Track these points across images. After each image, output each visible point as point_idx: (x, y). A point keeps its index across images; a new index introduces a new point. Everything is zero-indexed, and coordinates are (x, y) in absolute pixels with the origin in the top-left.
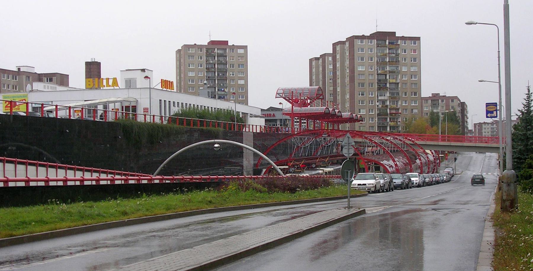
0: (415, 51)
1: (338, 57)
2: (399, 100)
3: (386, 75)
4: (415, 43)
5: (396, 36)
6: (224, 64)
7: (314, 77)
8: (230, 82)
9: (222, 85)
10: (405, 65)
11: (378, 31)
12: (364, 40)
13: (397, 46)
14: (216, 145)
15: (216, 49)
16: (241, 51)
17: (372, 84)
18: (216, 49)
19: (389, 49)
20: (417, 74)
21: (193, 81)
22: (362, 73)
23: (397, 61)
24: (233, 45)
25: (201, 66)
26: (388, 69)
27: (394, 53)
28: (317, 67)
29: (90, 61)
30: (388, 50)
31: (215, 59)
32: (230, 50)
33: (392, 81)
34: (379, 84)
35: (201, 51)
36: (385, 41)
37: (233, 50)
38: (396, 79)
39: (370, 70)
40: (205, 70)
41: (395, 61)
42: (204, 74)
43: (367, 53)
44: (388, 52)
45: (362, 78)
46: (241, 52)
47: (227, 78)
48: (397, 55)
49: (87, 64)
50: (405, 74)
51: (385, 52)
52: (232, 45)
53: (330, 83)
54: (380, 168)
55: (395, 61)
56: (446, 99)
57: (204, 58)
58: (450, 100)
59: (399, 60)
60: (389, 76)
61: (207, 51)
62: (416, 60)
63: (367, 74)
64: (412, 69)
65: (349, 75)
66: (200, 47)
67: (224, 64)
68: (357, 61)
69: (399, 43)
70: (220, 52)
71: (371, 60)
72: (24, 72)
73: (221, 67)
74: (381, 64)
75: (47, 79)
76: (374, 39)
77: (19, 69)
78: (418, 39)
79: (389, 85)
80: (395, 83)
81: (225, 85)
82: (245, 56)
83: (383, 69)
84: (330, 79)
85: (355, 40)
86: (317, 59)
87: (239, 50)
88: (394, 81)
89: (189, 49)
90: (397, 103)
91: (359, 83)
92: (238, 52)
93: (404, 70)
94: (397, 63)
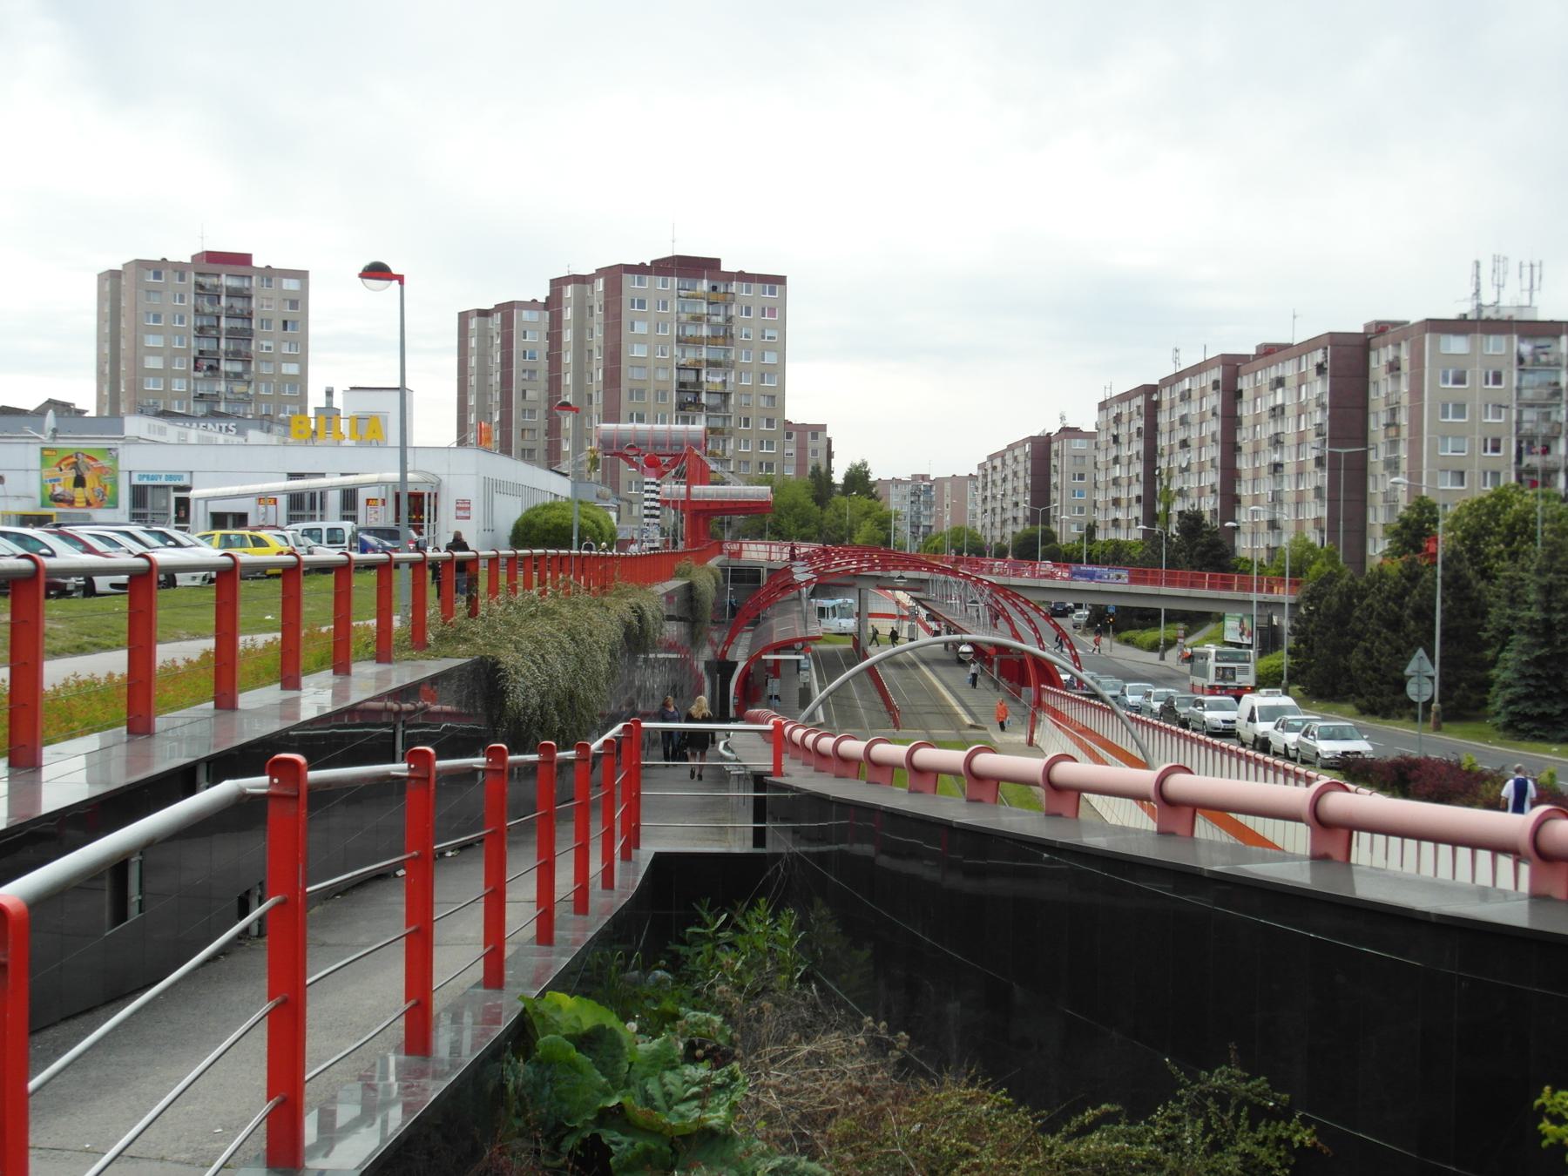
0: (772, 312)
1: (568, 314)
2: (730, 438)
4: (772, 292)
5: (722, 269)
11: (676, 254)
12: (647, 277)
17: (664, 394)
19: (709, 303)
22: (640, 364)
24: (269, 267)
25: (181, 321)
28: (484, 335)
30: (705, 305)
31: (219, 303)
32: (263, 280)
35: (182, 278)
37: (269, 280)
39: (659, 356)
40: (193, 332)
42: (189, 344)
45: (636, 374)
46: (291, 281)
48: (729, 319)
52: (263, 266)
53: (524, 380)
54: (489, 589)
55: (724, 336)
56: (797, 431)
58: (809, 434)
59: (734, 332)
66: (180, 269)
73: (238, 324)
78: (781, 280)
79: (707, 398)
82: (298, 303)
84: (524, 371)
86: (483, 314)
90: (724, 446)
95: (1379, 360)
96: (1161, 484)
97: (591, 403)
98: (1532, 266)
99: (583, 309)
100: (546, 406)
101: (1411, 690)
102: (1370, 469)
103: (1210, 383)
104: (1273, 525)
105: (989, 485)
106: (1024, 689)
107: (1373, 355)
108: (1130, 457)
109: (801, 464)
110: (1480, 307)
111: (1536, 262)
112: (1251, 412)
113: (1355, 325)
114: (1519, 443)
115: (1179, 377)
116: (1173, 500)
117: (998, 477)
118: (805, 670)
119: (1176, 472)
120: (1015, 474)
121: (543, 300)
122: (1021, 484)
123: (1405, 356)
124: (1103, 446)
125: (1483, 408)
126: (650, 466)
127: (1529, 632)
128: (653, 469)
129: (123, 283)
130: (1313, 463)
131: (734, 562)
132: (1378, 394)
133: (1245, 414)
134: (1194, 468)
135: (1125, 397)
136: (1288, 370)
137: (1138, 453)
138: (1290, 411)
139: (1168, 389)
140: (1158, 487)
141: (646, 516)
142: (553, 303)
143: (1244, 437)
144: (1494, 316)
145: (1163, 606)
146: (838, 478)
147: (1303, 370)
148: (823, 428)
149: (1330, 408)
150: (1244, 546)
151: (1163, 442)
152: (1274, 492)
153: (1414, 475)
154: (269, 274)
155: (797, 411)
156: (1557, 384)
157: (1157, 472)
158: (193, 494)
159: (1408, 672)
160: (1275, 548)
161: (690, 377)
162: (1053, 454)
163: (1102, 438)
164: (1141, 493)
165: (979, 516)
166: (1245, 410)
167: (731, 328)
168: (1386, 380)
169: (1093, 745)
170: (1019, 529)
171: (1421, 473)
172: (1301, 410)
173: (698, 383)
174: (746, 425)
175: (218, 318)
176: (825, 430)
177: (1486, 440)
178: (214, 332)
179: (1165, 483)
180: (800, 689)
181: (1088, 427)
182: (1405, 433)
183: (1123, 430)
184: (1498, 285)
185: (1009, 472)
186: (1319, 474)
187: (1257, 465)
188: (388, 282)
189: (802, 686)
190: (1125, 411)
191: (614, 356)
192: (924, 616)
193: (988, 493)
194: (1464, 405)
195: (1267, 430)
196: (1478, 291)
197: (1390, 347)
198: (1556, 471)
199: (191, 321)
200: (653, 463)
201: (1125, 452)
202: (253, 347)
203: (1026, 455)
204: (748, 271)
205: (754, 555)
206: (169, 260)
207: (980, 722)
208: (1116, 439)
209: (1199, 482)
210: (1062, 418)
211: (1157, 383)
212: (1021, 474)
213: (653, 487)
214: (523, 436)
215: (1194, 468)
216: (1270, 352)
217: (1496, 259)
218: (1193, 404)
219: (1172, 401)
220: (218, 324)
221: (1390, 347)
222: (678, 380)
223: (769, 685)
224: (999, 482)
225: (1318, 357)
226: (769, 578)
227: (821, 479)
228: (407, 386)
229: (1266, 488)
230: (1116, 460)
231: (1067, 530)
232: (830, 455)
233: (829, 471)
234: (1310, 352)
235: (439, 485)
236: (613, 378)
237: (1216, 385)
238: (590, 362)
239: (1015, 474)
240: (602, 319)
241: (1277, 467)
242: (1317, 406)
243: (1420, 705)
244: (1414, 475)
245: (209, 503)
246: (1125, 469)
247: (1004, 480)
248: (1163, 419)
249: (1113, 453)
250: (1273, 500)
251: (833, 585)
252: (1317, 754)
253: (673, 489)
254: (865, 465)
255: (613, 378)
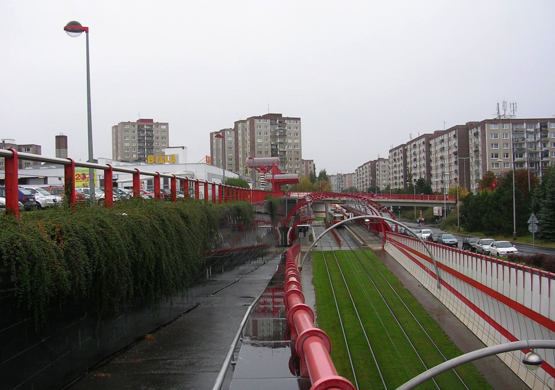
0: (297, 128)
1: (240, 132)
3: (277, 146)
4: (297, 123)
6: (151, 137)
7: (214, 146)
8: (156, 150)
9: (149, 152)
10: (290, 138)
13: (285, 124)
14: (367, 220)
15: (145, 126)
16: (164, 127)
17: (267, 152)
18: (145, 126)
19: (279, 126)
20: (299, 145)
21: (128, 150)
22: (260, 144)
23: (285, 136)
25: (134, 139)
26: (278, 141)
27: (282, 130)
29: (58, 135)
30: (278, 127)
33: (281, 150)
34: (272, 152)
35: (134, 127)
36: (276, 121)
37: (158, 126)
38: (284, 149)
41: (283, 135)
42: (136, 145)
43: (263, 129)
44: (278, 128)
45: (260, 147)
46: (164, 128)
47: (153, 147)
49: (57, 137)
50: (290, 145)
51: (276, 129)
52: (156, 122)
55: (283, 136)
57: (136, 132)
58: (309, 163)
60: (279, 146)
61: (138, 127)
62: (298, 135)
63: (264, 145)
64: (296, 141)
65: (249, 145)
66: (133, 124)
67: (151, 137)
68: (257, 135)
69: (286, 122)
70: (148, 127)
71: (267, 135)
72: (9, 144)
73: (150, 139)
74: (274, 137)
75: (25, 149)
76: (268, 119)
77: (4, 142)
78: (299, 119)
80: (283, 151)
81: (152, 153)
82: (166, 131)
83: (275, 141)
84: (229, 148)
85: (255, 120)
87: (162, 126)
88: (283, 150)
89: (125, 125)
91: (258, 152)
92: (162, 128)
93: (259, 142)
94: (285, 137)
95: (471, 133)
96: (408, 172)
97: (247, 156)
98: (513, 104)
99: (244, 130)
100: (235, 158)
101: (530, 228)
102: (470, 164)
103: (422, 142)
104: (442, 182)
105: (359, 175)
106: (380, 233)
107: (470, 131)
108: (399, 165)
109: (307, 171)
110: (500, 116)
111: (514, 103)
112: (434, 150)
113: (463, 122)
114: (514, 155)
115: (412, 141)
116: (412, 176)
117: (361, 173)
118: (310, 229)
119: (413, 168)
120: (366, 172)
121: (233, 128)
122: (368, 174)
123: (479, 131)
124: (391, 162)
125: (503, 145)
126: (262, 170)
127: (547, 207)
128: (263, 171)
129: (118, 128)
130: (454, 163)
131: (288, 197)
132: (472, 142)
133: (432, 150)
134: (418, 167)
135: (397, 148)
136: (445, 137)
137: (401, 164)
138: (446, 149)
139: (409, 145)
140: (408, 173)
141: (261, 185)
142: (236, 129)
143: (433, 157)
144: (504, 119)
145: (415, 205)
146: (317, 175)
147: (449, 137)
148: (312, 161)
149: (458, 147)
150: (434, 188)
151: (408, 160)
152: (442, 172)
153: (484, 166)
154: (158, 124)
155: (305, 156)
156: (523, 137)
157: (407, 169)
158: (117, 181)
159: (529, 222)
160: (443, 188)
161: (275, 147)
162: (376, 166)
163: (391, 160)
164: (403, 175)
165: (356, 184)
166: (432, 150)
167: (285, 133)
168: (474, 138)
169: (406, 250)
170: (368, 187)
171: (486, 164)
172: (449, 148)
173: (277, 149)
174: (291, 160)
175: (144, 137)
176: (313, 161)
177: (504, 154)
178: (143, 141)
179: (410, 172)
180: (309, 235)
181: (387, 157)
182: (480, 153)
183: (397, 157)
184: (505, 110)
185: (364, 171)
186: (456, 166)
187: (437, 165)
188: (80, 33)
189: (310, 234)
190: (397, 152)
191: (253, 142)
192: (345, 212)
193: (359, 178)
194: (498, 144)
195: (439, 155)
196: (499, 112)
197: (475, 129)
198: (525, 162)
199: (137, 138)
200: (263, 169)
201: (397, 164)
202: (154, 145)
203: (369, 166)
204: (289, 117)
205: (294, 195)
206: (131, 122)
207: (366, 243)
208: (395, 160)
209: (420, 171)
210: (379, 156)
211: (406, 143)
212: (368, 172)
213: (263, 176)
214: (229, 166)
215: (418, 167)
216: (438, 134)
217: (504, 102)
218: (417, 149)
219: (411, 148)
220: (144, 138)
221: (475, 129)
222: (271, 148)
223: (300, 234)
224: (361, 174)
225: (454, 133)
226: (299, 202)
227: (312, 177)
228: (223, 170)
229: (440, 171)
230: (395, 166)
231: (382, 188)
232: (315, 169)
233: (315, 173)
234: (451, 131)
235: (193, 175)
236: (253, 148)
237: (424, 143)
238: (246, 145)
239: (366, 172)
240: (249, 132)
241: (442, 166)
242: (455, 147)
243: (533, 234)
244: (484, 166)
245: (123, 184)
246: (398, 168)
247: (363, 173)
248: (408, 154)
249: (394, 164)
250: (442, 174)
251: (318, 203)
252: (483, 250)
253: (269, 176)
254: (324, 170)
255: (253, 148)
